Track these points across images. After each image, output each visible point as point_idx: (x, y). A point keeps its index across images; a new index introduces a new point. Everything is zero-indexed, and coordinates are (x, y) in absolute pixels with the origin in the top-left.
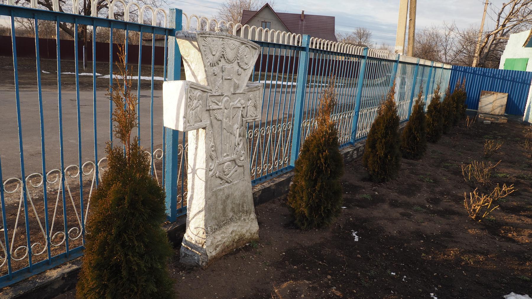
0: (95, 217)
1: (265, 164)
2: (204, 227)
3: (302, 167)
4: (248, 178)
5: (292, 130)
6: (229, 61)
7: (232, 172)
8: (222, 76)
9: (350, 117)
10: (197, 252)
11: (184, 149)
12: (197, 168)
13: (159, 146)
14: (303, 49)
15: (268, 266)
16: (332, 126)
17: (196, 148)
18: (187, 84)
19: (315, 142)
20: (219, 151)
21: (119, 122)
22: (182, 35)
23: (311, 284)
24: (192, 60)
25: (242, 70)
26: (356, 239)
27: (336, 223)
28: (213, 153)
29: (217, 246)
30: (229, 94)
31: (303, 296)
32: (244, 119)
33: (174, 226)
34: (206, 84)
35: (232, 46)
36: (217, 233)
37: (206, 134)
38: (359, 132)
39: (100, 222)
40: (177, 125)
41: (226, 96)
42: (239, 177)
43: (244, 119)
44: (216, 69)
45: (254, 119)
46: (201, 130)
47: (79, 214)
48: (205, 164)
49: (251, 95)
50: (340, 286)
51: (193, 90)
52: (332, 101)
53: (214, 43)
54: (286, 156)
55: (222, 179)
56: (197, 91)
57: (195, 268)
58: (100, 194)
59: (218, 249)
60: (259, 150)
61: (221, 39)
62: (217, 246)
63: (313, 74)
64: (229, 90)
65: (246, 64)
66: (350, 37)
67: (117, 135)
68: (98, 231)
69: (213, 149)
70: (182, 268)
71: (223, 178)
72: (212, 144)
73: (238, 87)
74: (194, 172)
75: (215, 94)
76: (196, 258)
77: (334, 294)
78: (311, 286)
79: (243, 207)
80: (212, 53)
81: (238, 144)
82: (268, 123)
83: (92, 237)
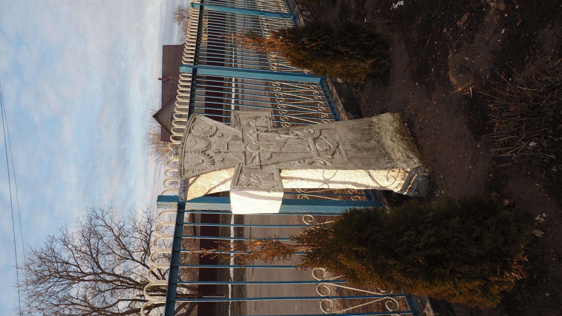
0: (376, 282)
1: (317, 110)
2: (387, 171)
3: (321, 67)
4: (334, 125)
5: (281, 81)
6: (209, 146)
7: (326, 141)
8: (225, 152)
9: (266, 20)
10: (415, 178)
11: (303, 193)
12: (322, 179)
13: (300, 218)
14: (195, 71)
15: (431, 100)
16: (276, 35)
17: (302, 179)
18: (234, 188)
19: (293, 54)
20: (305, 155)
21: (273, 256)
22: (183, 195)
23: (453, 51)
24: (208, 184)
25: (218, 132)
26: (402, 3)
27: (382, 27)
28: (307, 162)
29: (408, 157)
30: (243, 145)
31: (467, 59)
32: (270, 130)
33: (385, 203)
34: (233, 169)
35: (194, 143)
36: (393, 156)
37: (286, 169)
38: (282, 10)
39: (381, 277)
40: (277, 199)
41: (246, 149)
42: (332, 135)
43: (270, 130)
44: (217, 158)
45: (270, 119)
46: (282, 175)
47: (370, 300)
48: (318, 170)
49: (244, 123)
50: (455, 16)
51: (239, 183)
52: (247, 36)
53: (190, 161)
54: (309, 87)
55: (335, 152)
56: (241, 178)
57: (432, 180)
58: (352, 277)
59: (411, 156)
60: (303, 116)
61: (186, 154)
62: (408, 157)
63: (223, 60)
64: (240, 145)
65: (211, 128)
66: (183, 29)
67: (288, 258)
68: (390, 279)
69: (302, 162)
70: (431, 194)
71: (333, 151)
72: (297, 162)
73: (236, 136)
74: (327, 181)
75: (244, 160)
76: (420, 179)
77: (466, 22)
78: (455, 50)
79: (364, 130)
80: (200, 164)
81: (297, 135)
82: (274, 106)
83: (398, 285)
